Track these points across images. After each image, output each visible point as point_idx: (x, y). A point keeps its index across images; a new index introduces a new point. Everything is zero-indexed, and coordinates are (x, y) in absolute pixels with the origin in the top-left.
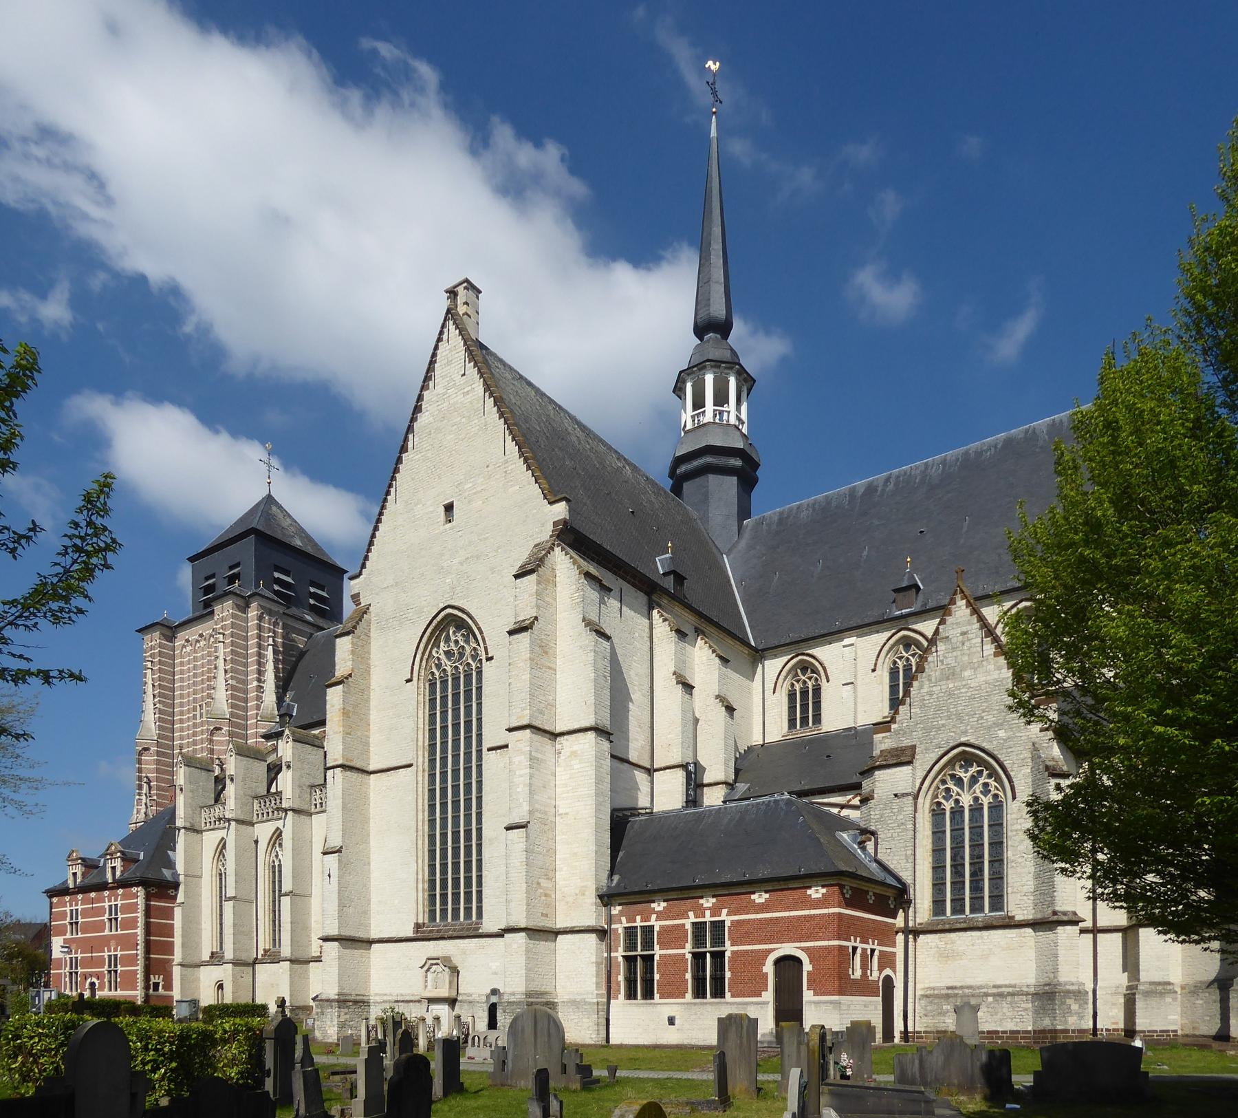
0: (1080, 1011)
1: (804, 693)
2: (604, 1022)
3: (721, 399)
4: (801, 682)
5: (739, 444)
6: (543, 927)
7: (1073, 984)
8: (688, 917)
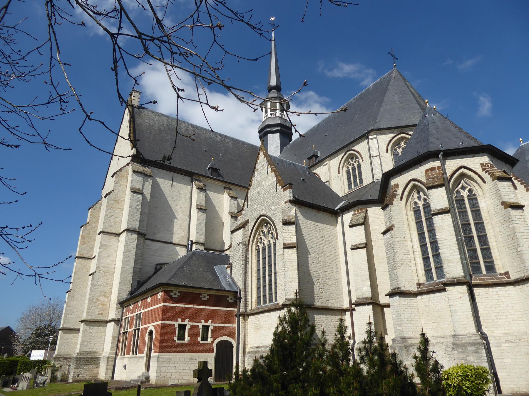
1: (354, 169)
2: (112, 367)
4: (351, 165)
5: (278, 122)
6: (98, 319)
8: (177, 321)
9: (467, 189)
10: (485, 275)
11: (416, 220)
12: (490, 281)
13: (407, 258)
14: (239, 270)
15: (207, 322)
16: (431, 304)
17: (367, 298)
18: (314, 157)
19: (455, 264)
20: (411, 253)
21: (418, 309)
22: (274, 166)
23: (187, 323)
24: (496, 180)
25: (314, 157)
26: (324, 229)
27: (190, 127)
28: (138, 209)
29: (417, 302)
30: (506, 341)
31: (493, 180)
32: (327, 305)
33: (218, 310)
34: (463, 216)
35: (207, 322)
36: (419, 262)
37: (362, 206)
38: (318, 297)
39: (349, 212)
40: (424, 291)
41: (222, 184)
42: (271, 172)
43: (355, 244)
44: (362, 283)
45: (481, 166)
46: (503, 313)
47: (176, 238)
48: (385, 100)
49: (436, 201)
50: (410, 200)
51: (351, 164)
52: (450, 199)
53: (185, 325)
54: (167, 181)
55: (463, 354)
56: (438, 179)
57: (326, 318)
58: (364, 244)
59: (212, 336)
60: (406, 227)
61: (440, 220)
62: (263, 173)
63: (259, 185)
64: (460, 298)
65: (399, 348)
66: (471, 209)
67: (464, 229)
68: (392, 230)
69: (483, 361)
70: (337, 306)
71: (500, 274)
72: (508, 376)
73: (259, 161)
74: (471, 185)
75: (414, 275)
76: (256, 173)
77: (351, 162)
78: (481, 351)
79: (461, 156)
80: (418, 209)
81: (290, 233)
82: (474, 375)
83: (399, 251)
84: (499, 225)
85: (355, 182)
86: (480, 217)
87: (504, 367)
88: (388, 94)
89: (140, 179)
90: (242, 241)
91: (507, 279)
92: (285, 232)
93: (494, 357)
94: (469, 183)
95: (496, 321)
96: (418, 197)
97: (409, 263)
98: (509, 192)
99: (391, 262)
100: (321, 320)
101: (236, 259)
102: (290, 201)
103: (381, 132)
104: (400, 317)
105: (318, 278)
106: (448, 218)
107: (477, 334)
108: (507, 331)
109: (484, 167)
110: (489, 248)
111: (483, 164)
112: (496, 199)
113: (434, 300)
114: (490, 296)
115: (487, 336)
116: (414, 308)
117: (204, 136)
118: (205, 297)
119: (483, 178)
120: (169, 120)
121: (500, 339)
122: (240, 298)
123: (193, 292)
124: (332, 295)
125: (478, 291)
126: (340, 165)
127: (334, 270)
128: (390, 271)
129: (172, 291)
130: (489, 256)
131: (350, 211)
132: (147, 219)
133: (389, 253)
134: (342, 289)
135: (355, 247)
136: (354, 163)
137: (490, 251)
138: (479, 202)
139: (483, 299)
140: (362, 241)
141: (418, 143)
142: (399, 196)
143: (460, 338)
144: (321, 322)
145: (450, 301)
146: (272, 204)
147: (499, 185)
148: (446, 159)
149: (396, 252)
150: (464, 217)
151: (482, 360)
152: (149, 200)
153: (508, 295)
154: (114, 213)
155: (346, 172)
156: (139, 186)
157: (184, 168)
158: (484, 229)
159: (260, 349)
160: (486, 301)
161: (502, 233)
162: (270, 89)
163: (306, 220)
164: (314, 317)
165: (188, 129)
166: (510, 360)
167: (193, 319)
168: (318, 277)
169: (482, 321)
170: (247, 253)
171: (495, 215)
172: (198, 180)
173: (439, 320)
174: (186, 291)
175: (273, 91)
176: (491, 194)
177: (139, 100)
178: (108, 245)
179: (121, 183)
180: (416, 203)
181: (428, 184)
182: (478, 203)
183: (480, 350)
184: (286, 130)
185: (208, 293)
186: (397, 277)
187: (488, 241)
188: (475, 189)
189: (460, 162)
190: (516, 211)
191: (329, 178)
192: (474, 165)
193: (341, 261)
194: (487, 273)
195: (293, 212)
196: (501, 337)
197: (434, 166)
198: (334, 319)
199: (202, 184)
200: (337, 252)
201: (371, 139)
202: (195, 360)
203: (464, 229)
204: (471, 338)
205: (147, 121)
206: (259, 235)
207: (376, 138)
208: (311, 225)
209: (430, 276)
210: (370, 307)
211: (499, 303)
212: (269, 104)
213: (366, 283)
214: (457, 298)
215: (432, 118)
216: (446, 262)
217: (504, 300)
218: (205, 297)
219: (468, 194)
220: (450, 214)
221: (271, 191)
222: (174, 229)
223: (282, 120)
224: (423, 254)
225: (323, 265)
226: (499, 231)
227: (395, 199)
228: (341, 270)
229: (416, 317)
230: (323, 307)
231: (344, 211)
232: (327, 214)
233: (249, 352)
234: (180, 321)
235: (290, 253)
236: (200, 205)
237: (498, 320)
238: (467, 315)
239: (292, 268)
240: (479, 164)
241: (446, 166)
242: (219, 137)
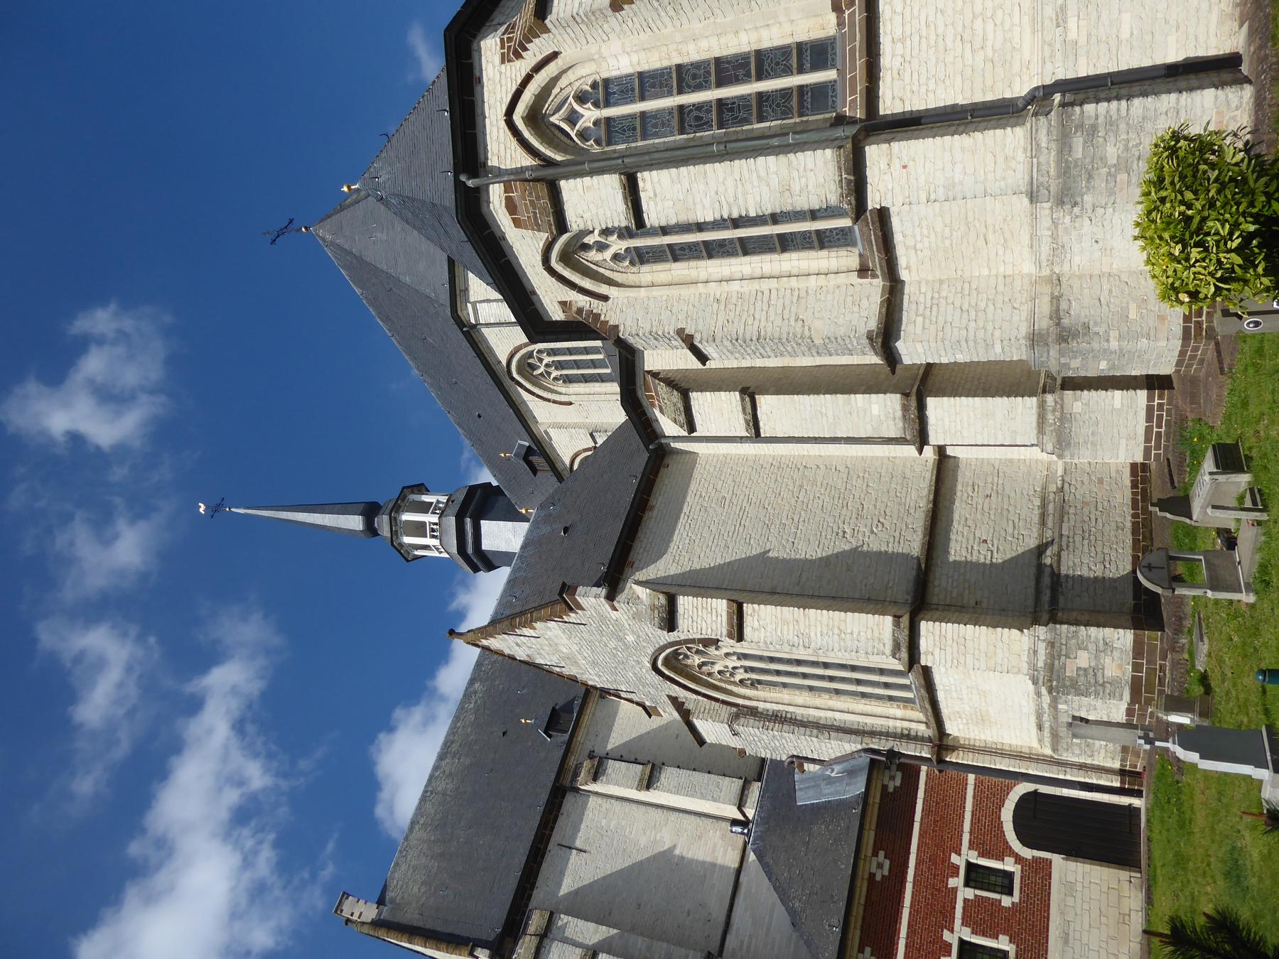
0: (1092, 647)
1: (560, 365)
3: (424, 508)
4: (549, 370)
5: (452, 521)
7: (1035, 652)
8: (955, 890)
9: (576, 107)
10: (841, 73)
11: (666, 261)
12: (860, 62)
13: (781, 301)
14: (808, 742)
15: (957, 868)
16: (927, 244)
17: (905, 408)
18: (530, 458)
19: (795, 174)
20: (766, 285)
21: (941, 282)
22: (518, 620)
23: (956, 936)
24: (547, 22)
25: (530, 458)
26: (701, 496)
27: (443, 763)
29: (920, 283)
30: (1058, 26)
31: (547, 31)
32: (923, 516)
33: (921, 825)
34: (655, 126)
35: (957, 868)
36: (795, 263)
37: (638, 384)
38: (897, 540)
39: (657, 420)
40: (884, 264)
41: (590, 704)
42: (534, 628)
43: (742, 422)
44: (858, 416)
45: (509, 61)
46: (964, 27)
47: (724, 855)
48: (385, 268)
49: (601, 212)
50: (608, 273)
51: (546, 371)
52: (597, 167)
53: (970, 866)
54: (570, 865)
55: (1096, 177)
56: (538, 198)
57: (959, 523)
58: (743, 400)
59: (1000, 858)
60: (686, 292)
61: (656, 204)
62: (539, 647)
63: (570, 658)
64: (904, 167)
65: (1063, 356)
66: (637, 99)
67: (696, 126)
68: (692, 337)
69: (1124, 113)
70: (927, 481)
71: (838, 25)
72: (1178, 28)
73: (507, 652)
74: (565, 93)
75: (832, 283)
76: (539, 661)
77: (542, 370)
78: (1090, 117)
79: (479, 120)
80: (633, 252)
81: (700, 613)
82: (1182, 195)
83: (756, 323)
84: (684, 19)
85: (594, 364)
86: (662, 75)
87: (1148, 38)
88: (369, 257)
90: (726, 726)
91: (856, 7)
92: (695, 629)
93: (1113, 68)
94: (558, 101)
95: (990, 53)
96: (597, 250)
97: (796, 294)
99: (789, 349)
100: (964, 540)
101: (778, 744)
102: (611, 597)
104: (963, 343)
105: (841, 534)
106: (649, 181)
107: (1028, 125)
108: (1026, 19)
109: (513, 52)
110: (758, 53)
111: (503, 54)
112: (606, 26)
113: (914, 236)
114: (907, 65)
115: (1037, 88)
116: (936, 295)
117: (469, 730)
118: (880, 866)
119: (542, 60)
120: (421, 822)
121: (1050, 45)
122: (892, 754)
123: (862, 901)
124: (892, 493)
125: (888, 102)
126: (549, 400)
127: (819, 479)
128: (818, 353)
130: (783, 56)
131: (654, 418)
132: (665, 945)
133: (762, 351)
134: (877, 458)
135: (751, 424)
136: (544, 362)
137: (766, 50)
138: (615, 73)
139: (915, 89)
140: (734, 403)
141: (446, 232)
142: (597, 306)
143: (1041, 179)
144: (971, 542)
145: (914, 200)
146: (620, 639)
147: (562, 15)
148: (485, 164)
149: (759, 332)
150: (660, 122)
151: (1119, 116)
152: (616, 931)
153: (908, 9)
155: (568, 384)
157: (540, 809)
158: (696, 65)
159: (1047, 725)
160: (923, 80)
161: (709, 14)
162: (371, 530)
163: (670, 550)
164: (955, 561)
165: (447, 772)
166: (1126, 18)
167: (944, 916)
168: (837, 534)
169: (989, 97)
170: (762, 713)
171: (655, 29)
172: (576, 774)
173: (977, 225)
175: (376, 525)
176: (591, 40)
177: (362, 902)
180: (616, 257)
181: (550, 229)
182: (619, 78)
183: (1086, 122)
184: (474, 503)
185: (869, 853)
186: (836, 338)
187: (736, 56)
188: (577, 84)
189: (495, 122)
191: (582, 431)
192: (503, 82)
193: (797, 453)
194: (833, 66)
195: (642, 592)
196: (1044, 42)
197: (504, 202)
198: (965, 495)
199: (587, 764)
200: (771, 461)
201: (476, 318)
202: (1071, 927)
203: (696, 126)
204: (1044, 145)
205: (416, 889)
206: (710, 674)
207: (474, 304)
208: (685, 535)
209: (839, 236)
210: (931, 402)
211: (933, 37)
212: (407, 540)
213: (860, 404)
214: (905, 175)
215: (384, 182)
216: (789, 201)
217: (923, 23)
218: (880, 866)
219: (589, 105)
220: (639, 175)
221: (586, 636)
222: (701, 858)
223: (448, 511)
224: (771, 250)
225: (802, 512)
226: (704, 23)
227: (602, 318)
228: (823, 454)
229: (966, 292)
230: (926, 529)
231: (654, 431)
232: (658, 480)
233: (1055, 750)
234: (956, 882)
235: (756, 624)
236: (641, 780)
237: (989, 44)
238: (963, 149)
239: (801, 624)
240: (503, 66)
241: (503, 167)
242: (477, 685)
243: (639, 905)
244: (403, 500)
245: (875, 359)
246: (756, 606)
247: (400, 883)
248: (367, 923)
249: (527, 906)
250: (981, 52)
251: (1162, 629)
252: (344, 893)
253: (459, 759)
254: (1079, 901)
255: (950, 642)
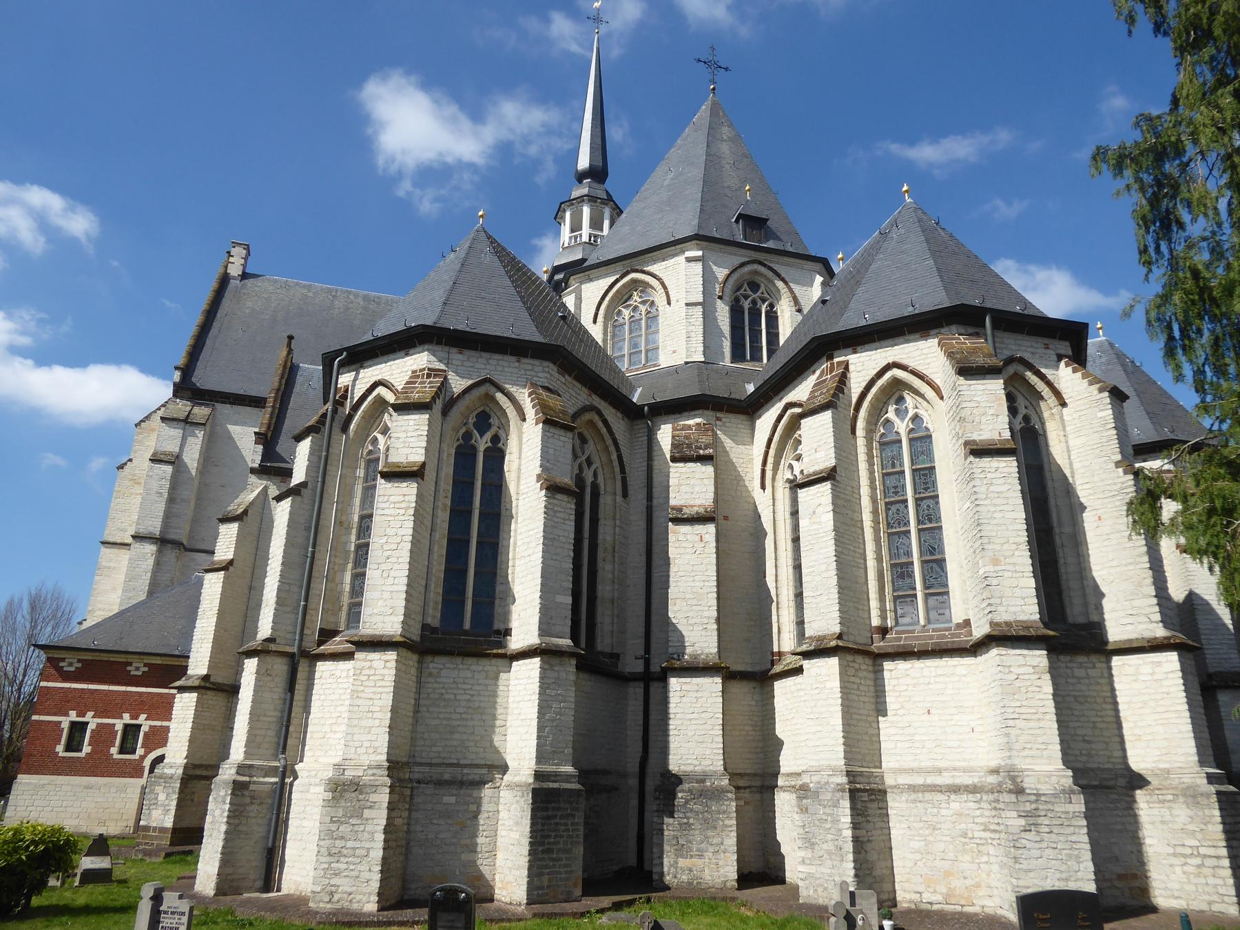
3: (596, 224)
8: (121, 718)
28: (161, 493)
35: (137, 719)
89: (175, 433)
98: (412, 439)
103: (588, 275)
106: (407, 492)
123: (111, 659)
129: (65, 659)
152: (194, 474)
154: (129, 503)
156: (172, 447)
162: (581, 177)
165: (350, 305)
174: (94, 658)
178: (114, 568)
179: (147, 443)
185: (145, 661)
190: (396, 485)
218: (138, 668)
234: (127, 718)
235: (213, 581)
243: (223, 486)
244: (602, 203)
245: (568, 642)
246: (222, 580)
247: (257, 289)
248: (226, 270)
249: (218, 402)
250: (329, 730)
251: (170, 845)
252: (248, 245)
253: (360, 314)
254: (113, 795)
255: (185, 713)
